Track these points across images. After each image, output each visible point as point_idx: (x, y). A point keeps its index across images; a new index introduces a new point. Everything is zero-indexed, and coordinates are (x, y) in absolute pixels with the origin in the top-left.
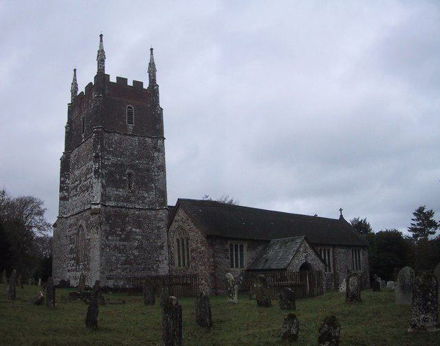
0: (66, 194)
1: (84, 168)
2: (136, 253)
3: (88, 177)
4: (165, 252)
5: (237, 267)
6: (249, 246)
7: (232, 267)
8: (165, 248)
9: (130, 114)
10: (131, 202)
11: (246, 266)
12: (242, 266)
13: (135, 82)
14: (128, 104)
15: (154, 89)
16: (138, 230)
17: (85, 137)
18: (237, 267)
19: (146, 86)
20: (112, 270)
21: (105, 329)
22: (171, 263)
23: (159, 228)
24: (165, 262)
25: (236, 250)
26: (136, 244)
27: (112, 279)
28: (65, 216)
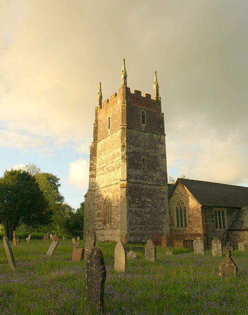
0: (94, 173)
1: (111, 154)
2: (148, 216)
3: (114, 161)
4: (167, 216)
5: (221, 228)
6: (227, 213)
7: (217, 227)
8: (167, 213)
9: (143, 116)
10: (145, 180)
11: (227, 228)
12: (224, 227)
13: (136, 91)
14: (142, 109)
15: (158, 102)
16: (149, 200)
17: (110, 132)
18: (221, 228)
19: (153, 97)
20: (133, 229)
21: (171, 216)
22: (172, 224)
23: (163, 199)
24: (167, 223)
25: (219, 215)
26: (148, 210)
27: (133, 235)
28: (93, 189)
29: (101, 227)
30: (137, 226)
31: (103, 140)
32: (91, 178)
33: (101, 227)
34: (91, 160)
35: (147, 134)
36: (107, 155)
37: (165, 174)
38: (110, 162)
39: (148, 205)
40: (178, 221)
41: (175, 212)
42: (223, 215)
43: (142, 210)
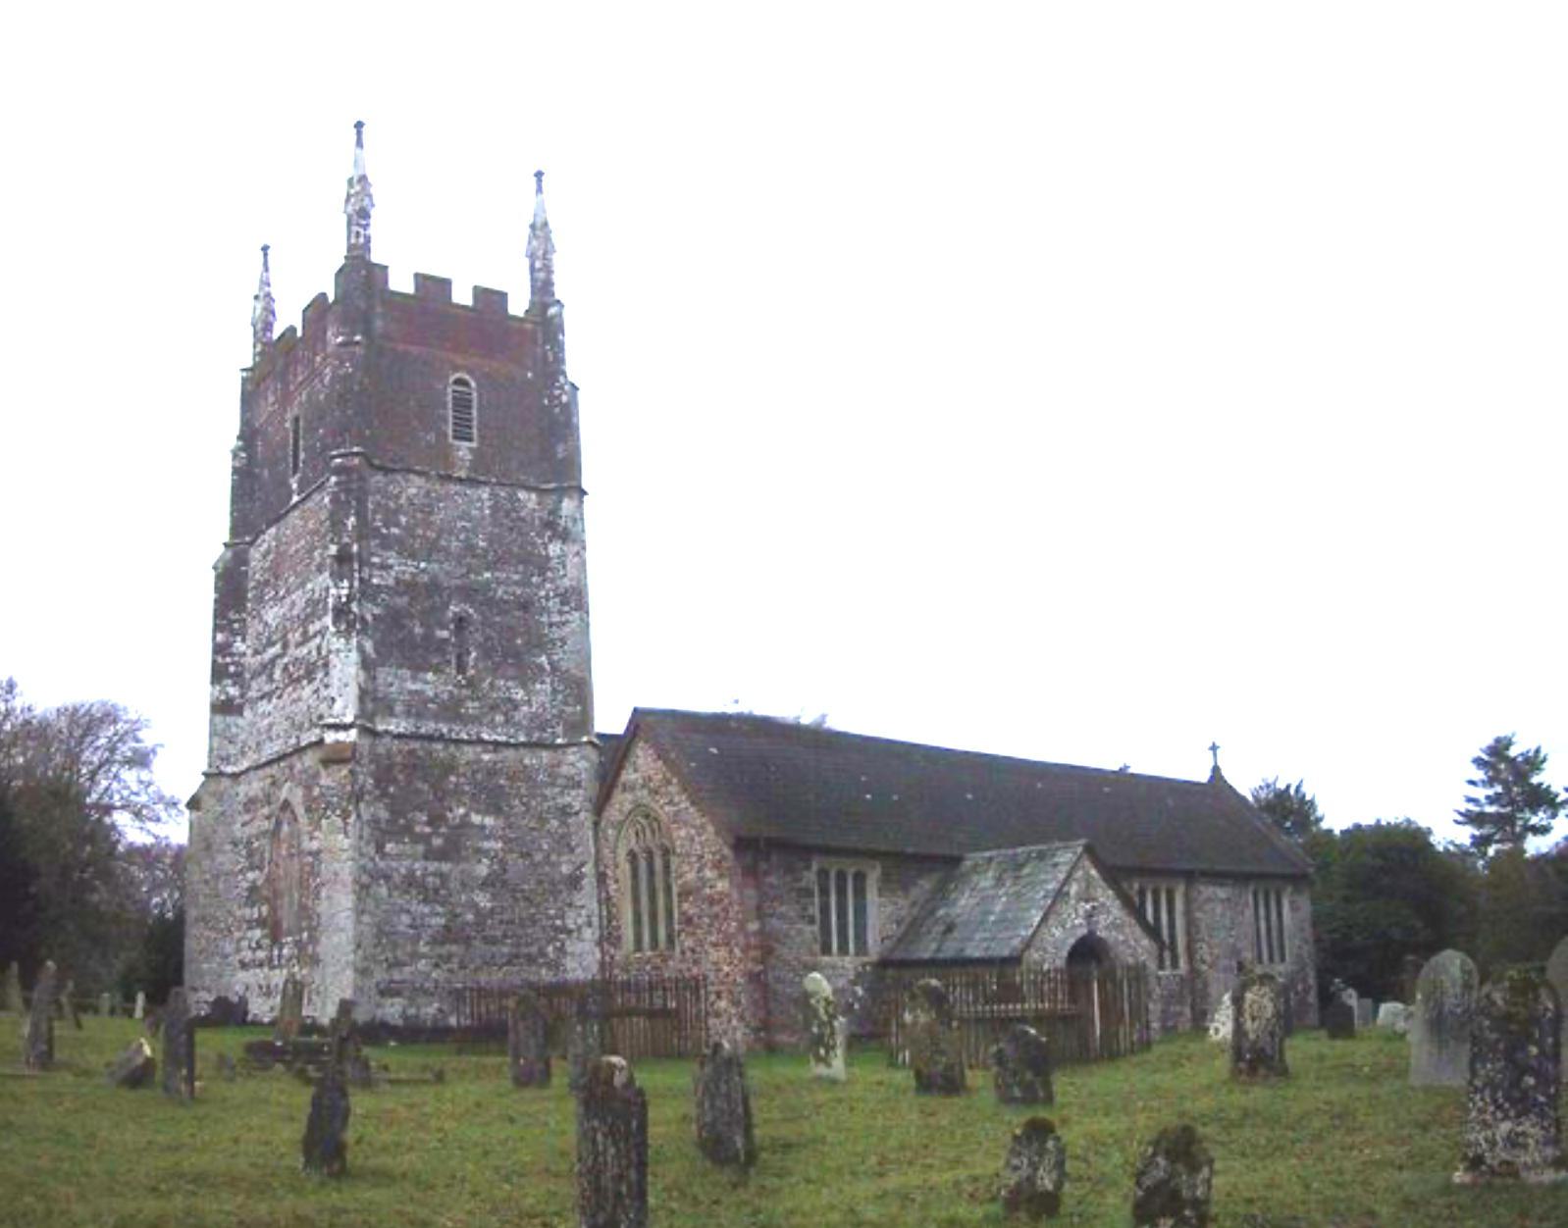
0: (233, 691)
1: (299, 598)
2: (483, 900)
3: (312, 629)
4: (587, 898)
7: (826, 949)
8: (589, 883)
9: (462, 404)
10: (476, 720)
11: (875, 949)
13: (480, 293)
14: (456, 369)
16: (489, 821)
18: (843, 949)
19: (518, 305)
20: (398, 964)
21: (609, 898)
23: (564, 812)
24: (587, 933)
26: (483, 869)
27: (398, 993)
28: (229, 769)
29: (261, 954)
30: (423, 949)
31: (273, 530)
32: (218, 719)
33: (261, 954)
34: (217, 628)
35: (485, 493)
36: (288, 601)
37: (578, 689)
38: (296, 636)
39: (486, 845)
40: (637, 921)
41: (626, 867)
42: (860, 892)
43: (446, 867)
